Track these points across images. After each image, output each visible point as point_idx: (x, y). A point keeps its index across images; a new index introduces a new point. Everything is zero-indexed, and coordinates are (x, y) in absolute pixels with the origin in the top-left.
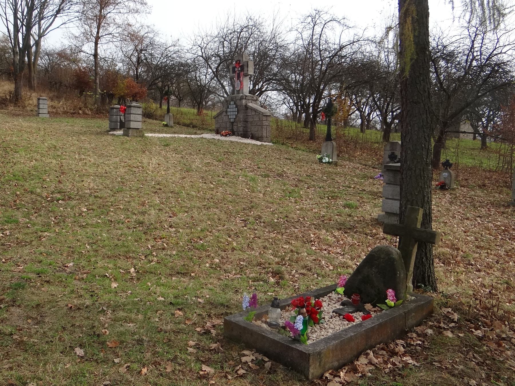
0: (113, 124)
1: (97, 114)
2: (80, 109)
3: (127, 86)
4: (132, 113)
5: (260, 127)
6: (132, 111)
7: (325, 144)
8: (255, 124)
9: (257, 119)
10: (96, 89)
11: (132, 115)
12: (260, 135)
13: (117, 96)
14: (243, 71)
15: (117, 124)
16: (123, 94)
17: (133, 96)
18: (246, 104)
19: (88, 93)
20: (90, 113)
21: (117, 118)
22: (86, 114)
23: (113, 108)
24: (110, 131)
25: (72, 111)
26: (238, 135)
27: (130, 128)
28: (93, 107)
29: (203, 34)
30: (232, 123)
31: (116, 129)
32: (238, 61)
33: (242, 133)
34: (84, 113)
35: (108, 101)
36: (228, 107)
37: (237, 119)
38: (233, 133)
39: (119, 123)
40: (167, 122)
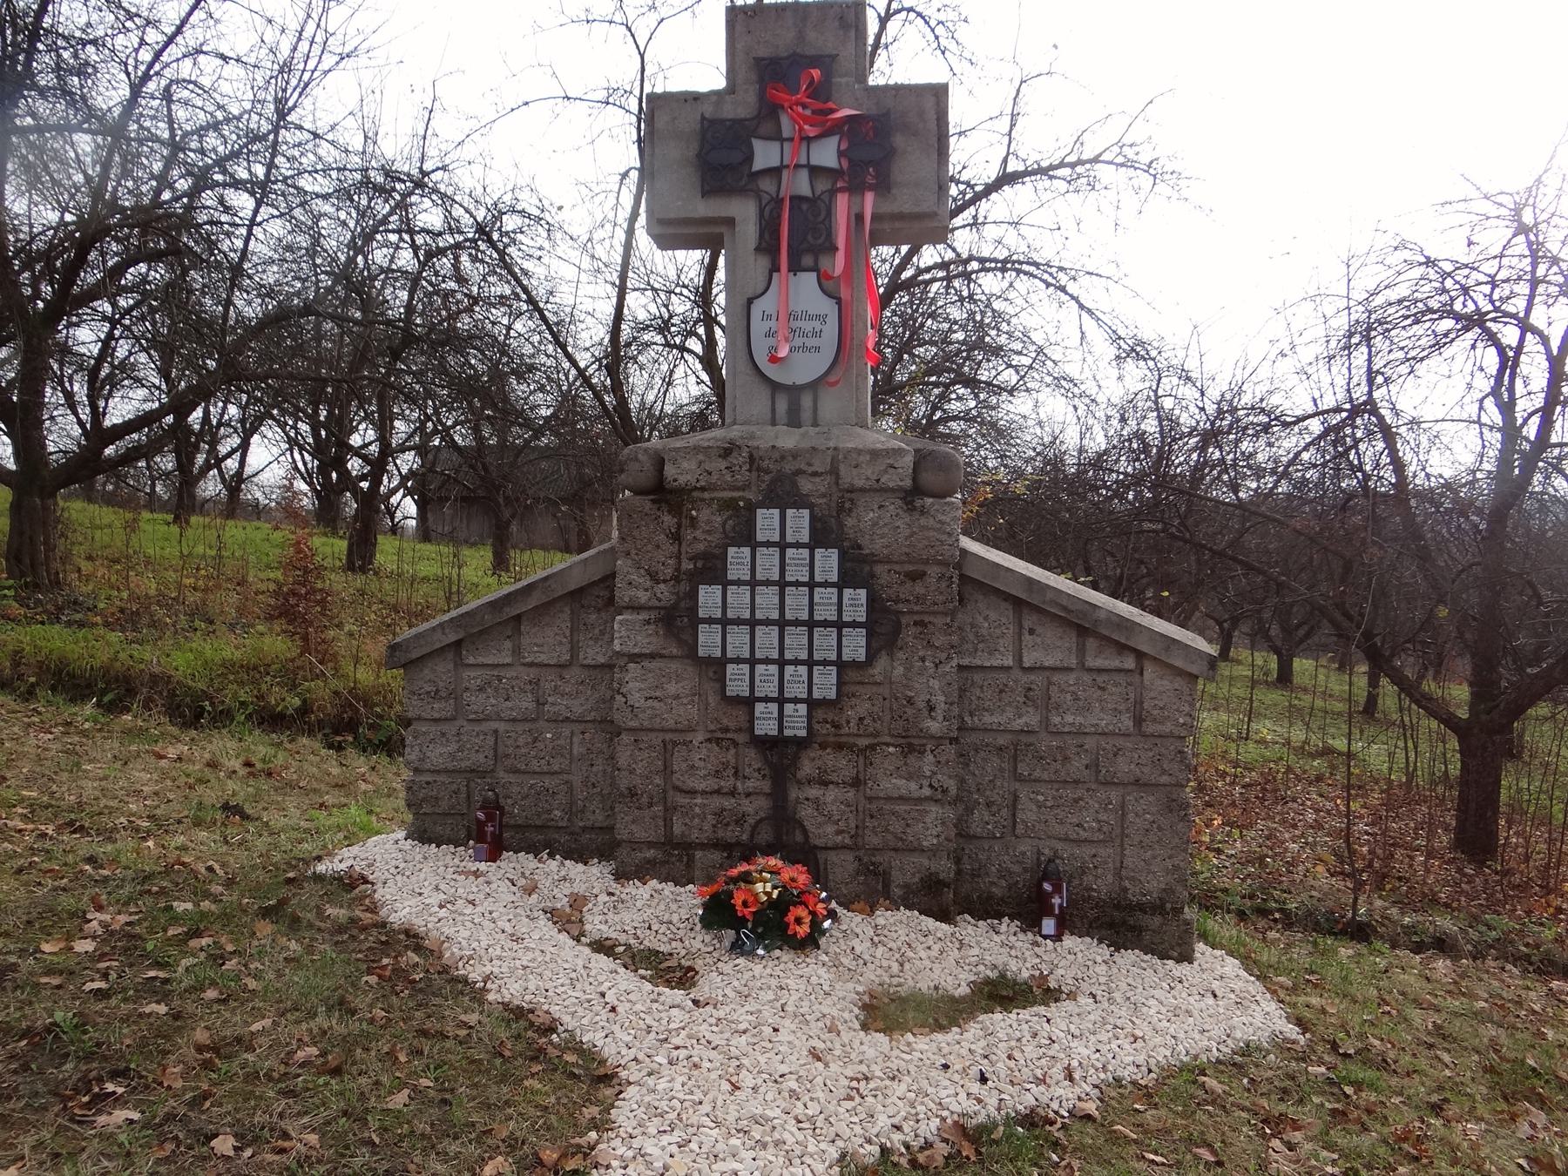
5: (1144, 808)
12: (1153, 884)
14: (883, 186)
33: (944, 867)
37: (856, 710)
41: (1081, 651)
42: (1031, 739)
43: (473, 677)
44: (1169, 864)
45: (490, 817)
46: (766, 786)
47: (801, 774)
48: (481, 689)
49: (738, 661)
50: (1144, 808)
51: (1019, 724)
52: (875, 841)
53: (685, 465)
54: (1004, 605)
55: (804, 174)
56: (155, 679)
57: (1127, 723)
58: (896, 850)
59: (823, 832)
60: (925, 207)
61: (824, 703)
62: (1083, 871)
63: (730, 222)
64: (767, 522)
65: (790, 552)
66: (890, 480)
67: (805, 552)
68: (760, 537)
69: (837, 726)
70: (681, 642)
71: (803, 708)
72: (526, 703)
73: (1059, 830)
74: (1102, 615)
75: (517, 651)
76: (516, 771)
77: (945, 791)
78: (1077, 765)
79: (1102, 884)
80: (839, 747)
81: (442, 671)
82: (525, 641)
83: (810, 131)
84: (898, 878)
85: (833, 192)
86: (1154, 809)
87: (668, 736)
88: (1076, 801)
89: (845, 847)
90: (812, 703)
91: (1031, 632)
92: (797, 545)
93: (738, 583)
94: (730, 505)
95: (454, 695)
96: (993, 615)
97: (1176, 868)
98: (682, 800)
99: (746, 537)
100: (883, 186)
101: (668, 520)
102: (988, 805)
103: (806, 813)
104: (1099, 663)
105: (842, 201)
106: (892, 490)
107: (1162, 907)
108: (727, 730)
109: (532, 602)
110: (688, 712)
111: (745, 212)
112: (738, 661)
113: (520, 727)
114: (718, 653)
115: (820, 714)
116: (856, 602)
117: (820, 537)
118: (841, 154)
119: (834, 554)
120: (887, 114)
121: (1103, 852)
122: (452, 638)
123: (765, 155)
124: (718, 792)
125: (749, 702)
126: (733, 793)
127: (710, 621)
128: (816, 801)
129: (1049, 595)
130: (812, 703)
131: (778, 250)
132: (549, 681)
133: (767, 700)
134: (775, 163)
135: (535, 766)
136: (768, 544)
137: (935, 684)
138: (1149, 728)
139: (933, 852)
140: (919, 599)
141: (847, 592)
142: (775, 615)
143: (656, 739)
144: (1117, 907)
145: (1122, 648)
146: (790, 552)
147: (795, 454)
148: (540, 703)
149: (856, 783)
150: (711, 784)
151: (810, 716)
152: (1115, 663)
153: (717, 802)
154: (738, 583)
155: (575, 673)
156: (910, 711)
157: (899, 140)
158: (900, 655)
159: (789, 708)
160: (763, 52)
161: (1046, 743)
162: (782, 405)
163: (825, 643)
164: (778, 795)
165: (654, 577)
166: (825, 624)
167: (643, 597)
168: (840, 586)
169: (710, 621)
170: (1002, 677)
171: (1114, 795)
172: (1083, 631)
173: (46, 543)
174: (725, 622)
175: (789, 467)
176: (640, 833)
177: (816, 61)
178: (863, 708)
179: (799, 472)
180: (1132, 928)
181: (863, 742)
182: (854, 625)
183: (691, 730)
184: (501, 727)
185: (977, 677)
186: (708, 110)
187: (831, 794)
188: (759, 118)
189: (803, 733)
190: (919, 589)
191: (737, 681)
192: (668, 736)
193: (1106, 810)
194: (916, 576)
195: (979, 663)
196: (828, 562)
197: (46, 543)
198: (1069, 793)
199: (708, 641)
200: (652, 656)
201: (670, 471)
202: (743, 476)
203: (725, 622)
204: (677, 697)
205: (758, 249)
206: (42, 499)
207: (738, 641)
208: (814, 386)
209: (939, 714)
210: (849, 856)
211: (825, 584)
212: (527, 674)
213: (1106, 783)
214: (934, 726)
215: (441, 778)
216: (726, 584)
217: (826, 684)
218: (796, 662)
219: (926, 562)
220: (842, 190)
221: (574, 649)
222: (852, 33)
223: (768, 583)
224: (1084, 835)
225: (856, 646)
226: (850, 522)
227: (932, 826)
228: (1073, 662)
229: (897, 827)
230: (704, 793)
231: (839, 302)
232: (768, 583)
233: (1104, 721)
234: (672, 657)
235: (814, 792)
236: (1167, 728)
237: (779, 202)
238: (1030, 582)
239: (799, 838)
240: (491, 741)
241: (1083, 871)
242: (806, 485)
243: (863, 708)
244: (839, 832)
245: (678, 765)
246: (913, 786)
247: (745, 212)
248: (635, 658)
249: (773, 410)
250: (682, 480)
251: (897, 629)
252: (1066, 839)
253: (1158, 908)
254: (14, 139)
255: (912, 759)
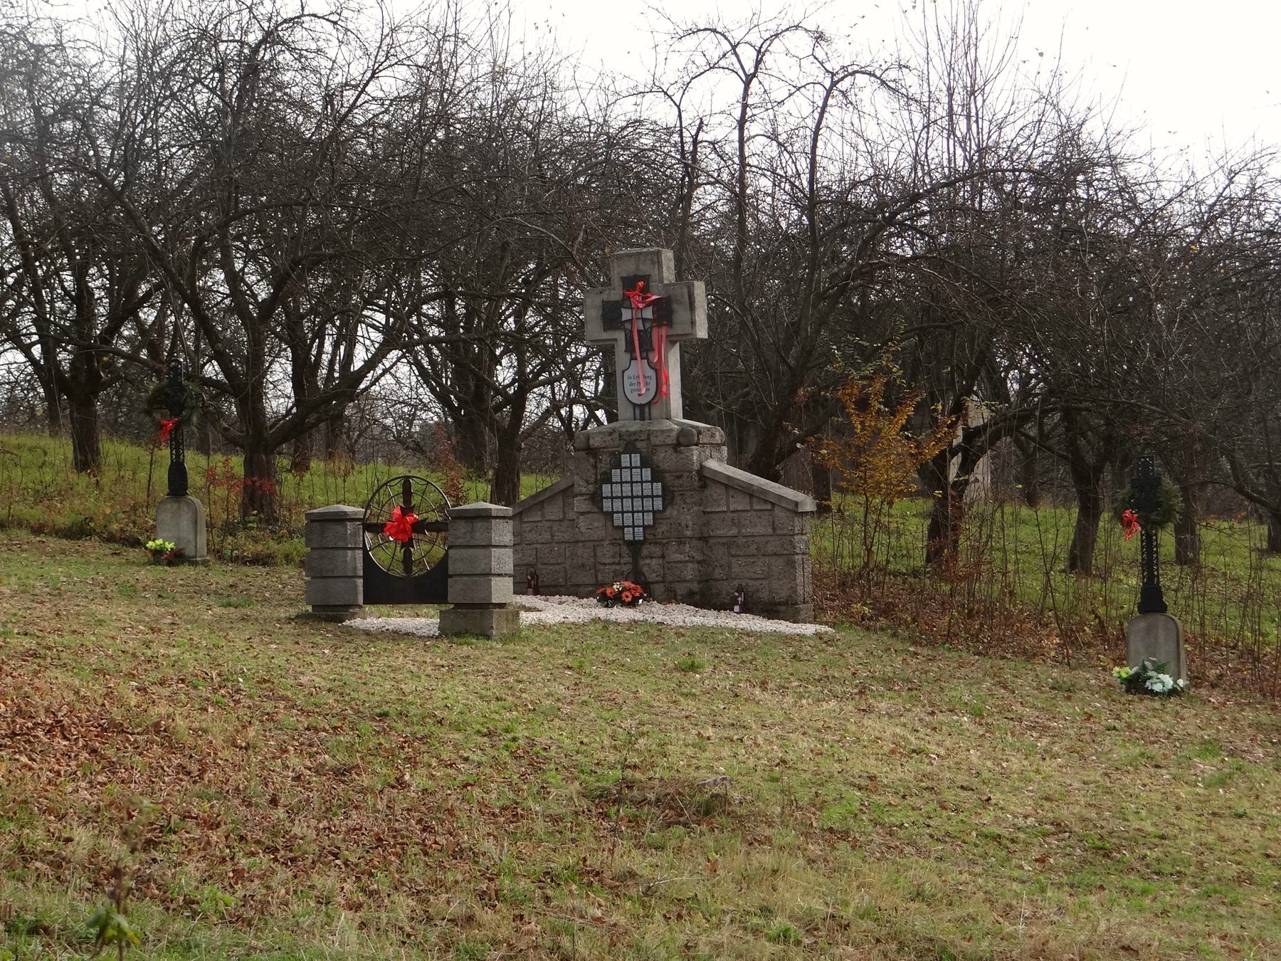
5: (778, 563)
7: (1142, 624)
8: (752, 549)
9: (761, 528)
12: (783, 594)
14: (670, 324)
15: (356, 586)
33: (695, 587)
36: (608, 479)
37: (662, 529)
38: (646, 590)
40: (178, 540)
41: (751, 504)
45: (533, 578)
46: (630, 560)
48: (530, 531)
49: (618, 512)
52: (670, 578)
57: (770, 530)
61: (649, 526)
62: (757, 591)
64: (625, 459)
66: (669, 441)
68: (623, 465)
70: (598, 507)
71: (641, 529)
72: (547, 536)
75: (543, 516)
76: (545, 564)
78: (752, 549)
83: (641, 306)
84: (679, 592)
85: (652, 328)
90: (645, 527)
92: (636, 468)
93: (616, 483)
94: (613, 453)
96: (718, 491)
98: (602, 567)
99: (618, 465)
101: (592, 460)
103: (645, 569)
104: (758, 507)
109: (548, 494)
110: (601, 533)
112: (618, 512)
113: (545, 546)
115: (648, 531)
116: (658, 487)
117: (644, 464)
119: (649, 470)
123: (626, 314)
124: (613, 563)
125: (622, 527)
126: (619, 564)
127: (607, 498)
130: (645, 527)
131: (635, 351)
133: (628, 527)
134: (629, 317)
135: (552, 561)
136: (626, 468)
137: (688, 517)
138: (779, 532)
139: (691, 581)
143: (591, 544)
145: (766, 501)
148: (553, 536)
149: (663, 557)
152: (764, 507)
153: (614, 567)
154: (616, 483)
155: (566, 523)
157: (675, 306)
159: (636, 529)
160: (624, 275)
161: (741, 541)
162: (638, 412)
164: (635, 563)
165: (587, 482)
166: (647, 497)
167: (584, 490)
168: (652, 482)
170: (722, 516)
171: (767, 559)
174: (612, 498)
175: (633, 438)
176: (587, 581)
179: (637, 440)
181: (664, 541)
183: (602, 540)
184: (539, 546)
185: (714, 516)
187: (654, 562)
194: (679, 477)
196: (647, 474)
198: (751, 560)
199: (607, 505)
200: (589, 513)
201: (591, 442)
202: (617, 442)
203: (612, 498)
206: (266, 455)
207: (617, 505)
208: (649, 404)
209: (690, 528)
210: (662, 585)
211: (647, 482)
214: (688, 533)
217: (649, 519)
218: (638, 512)
221: (564, 513)
223: (626, 482)
225: (658, 504)
226: (655, 458)
227: (690, 572)
228: (749, 508)
232: (626, 482)
233: (762, 531)
235: (647, 561)
237: (631, 332)
241: (757, 591)
242: (639, 445)
248: (583, 513)
250: (596, 445)
251: (673, 499)
252: (751, 579)
253: (786, 603)
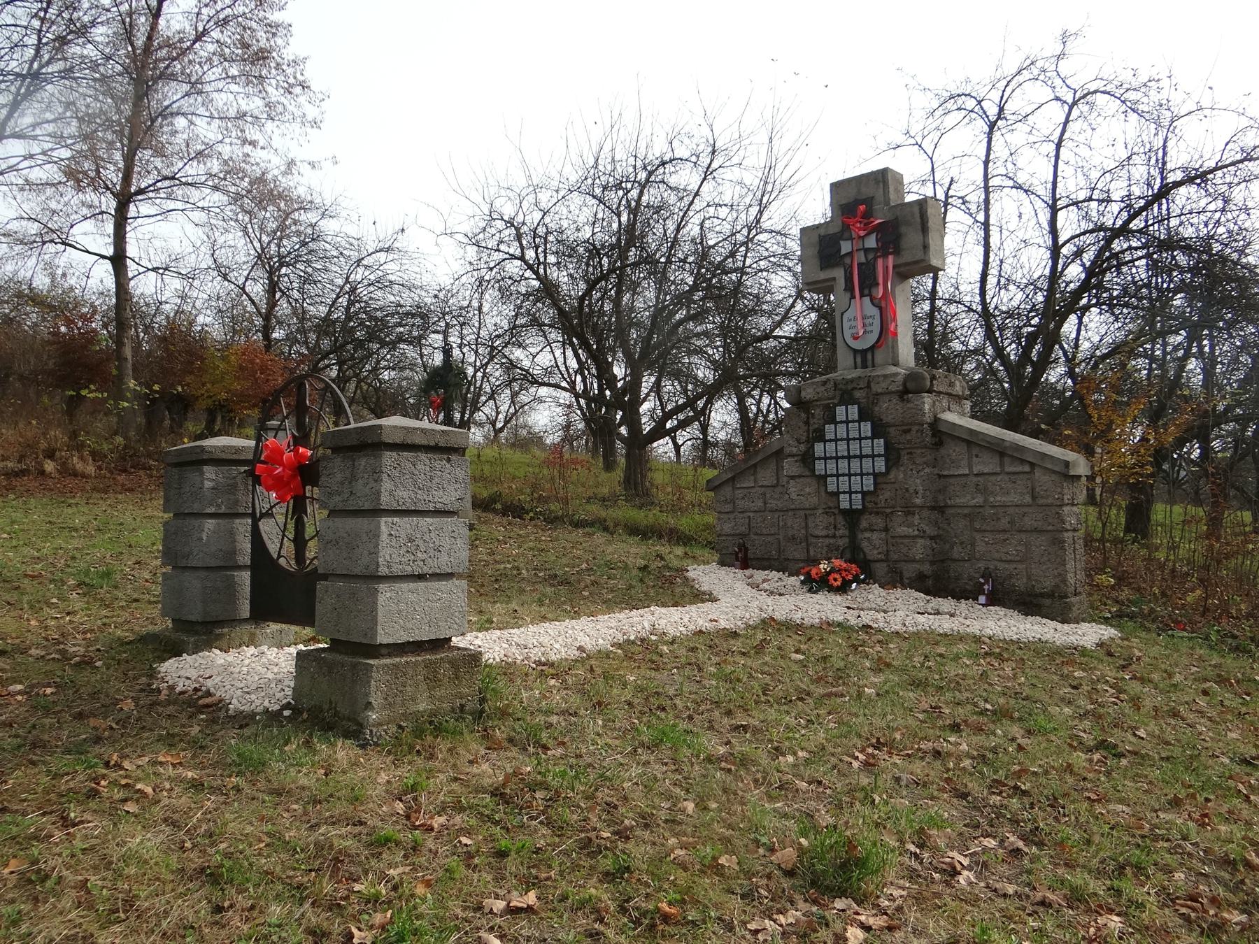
0: (194, 583)
1: (125, 471)
2: (50, 455)
3: (241, 368)
4: (385, 501)
6: (387, 485)
10: (120, 378)
11: (385, 524)
12: (1048, 583)
13: (202, 404)
14: (897, 252)
15: (231, 589)
16: (224, 396)
17: (265, 401)
18: (935, 417)
19: (84, 393)
20: (91, 469)
21: (232, 534)
22: (75, 474)
23: (199, 460)
24: (174, 650)
25: (10, 464)
26: (894, 580)
27: (375, 650)
28: (105, 447)
29: (520, 182)
30: (852, 516)
31: (220, 623)
32: (858, 202)
33: (927, 568)
34: (67, 471)
35: (167, 422)
36: (821, 437)
37: (886, 495)
39: (245, 577)
41: (1002, 465)
42: (981, 510)
43: (739, 493)
44: (1056, 572)
46: (847, 533)
47: (861, 527)
48: (743, 498)
50: (1040, 544)
51: (973, 502)
52: (896, 557)
53: (809, 391)
54: (963, 444)
55: (862, 253)
56: (671, 530)
57: (1028, 499)
58: (906, 561)
59: (872, 554)
60: (917, 258)
61: (869, 493)
63: (834, 279)
64: (840, 412)
65: (850, 425)
67: (857, 424)
68: (838, 419)
69: (876, 504)
71: (859, 496)
72: (760, 503)
73: (996, 555)
74: (1008, 444)
76: (757, 534)
77: (924, 532)
78: (1004, 522)
79: (1021, 583)
80: (877, 513)
81: (727, 491)
82: (759, 476)
83: (862, 233)
84: (906, 575)
85: (875, 259)
86: (1045, 544)
87: (807, 512)
88: (1005, 540)
89: (882, 561)
90: (864, 494)
91: (977, 456)
95: (733, 501)
96: (957, 449)
97: (1060, 575)
98: (814, 540)
99: (833, 420)
100: (897, 252)
102: (962, 543)
103: (865, 544)
104: (1012, 469)
105: (880, 262)
106: (893, 392)
107: (1053, 595)
108: (830, 508)
111: (839, 274)
113: (758, 514)
114: (823, 473)
117: (863, 417)
118: (877, 241)
119: (869, 424)
120: (897, 218)
121: (1020, 566)
122: (730, 476)
123: (846, 247)
124: (827, 536)
126: (834, 536)
127: (820, 459)
128: (869, 539)
129: (981, 437)
130: (864, 494)
132: (769, 493)
133: (844, 492)
136: (841, 422)
137: (918, 481)
138: (1041, 501)
139: (921, 561)
140: (909, 442)
141: (875, 441)
142: (846, 454)
143: (802, 513)
144: (1030, 595)
145: (1023, 461)
146: (850, 425)
147: (852, 381)
148: (765, 503)
150: (824, 533)
151: (863, 499)
152: (1019, 469)
153: (828, 541)
156: (907, 495)
157: (903, 229)
158: (902, 469)
162: (859, 360)
163: (867, 464)
164: (853, 537)
165: (798, 441)
167: (795, 450)
168: (872, 438)
169: (820, 459)
171: (1023, 536)
172: (1002, 454)
173: (641, 474)
176: (798, 556)
177: (863, 202)
178: (887, 494)
180: (1036, 605)
181: (889, 511)
182: (879, 456)
183: (815, 509)
184: (751, 515)
186: (822, 232)
187: (875, 536)
188: (842, 231)
189: (860, 507)
190: (908, 437)
191: (832, 484)
192: (807, 512)
193: (1020, 545)
195: (951, 473)
196: (867, 428)
197: (641, 474)
199: (819, 467)
200: (799, 476)
204: (809, 494)
205: (845, 290)
207: (831, 466)
208: (872, 348)
209: (920, 495)
212: (761, 490)
213: (1020, 531)
214: (918, 501)
215: (730, 538)
216: (825, 441)
217: (869, 483)
218: (856, 475)
219: (911, 424)
220: (879, 257)
222: (881, 185)
224: (1009, 558)
225: (880, 465)
226: (877, 409)
227: (920, 549)
228: (998, 470)
229: (904, 550)
230: (822, 537)
231: (881, 308)
234: (564, 389)
235: (867, 535)
236: (1050, 501)
238: (971, 431)
239: (862, 556)
240: (747, 520)
242: (857, 394)
243: (887, 494)
244: (879, 553)
245: (811, 525)
246: (911, 530)
247: (839, 274)
249: (855, 363)
250: (808, 397)
252: (1001, 561)
253: (1051, 595)
254: (1199, 305)
255: (910, 518)
